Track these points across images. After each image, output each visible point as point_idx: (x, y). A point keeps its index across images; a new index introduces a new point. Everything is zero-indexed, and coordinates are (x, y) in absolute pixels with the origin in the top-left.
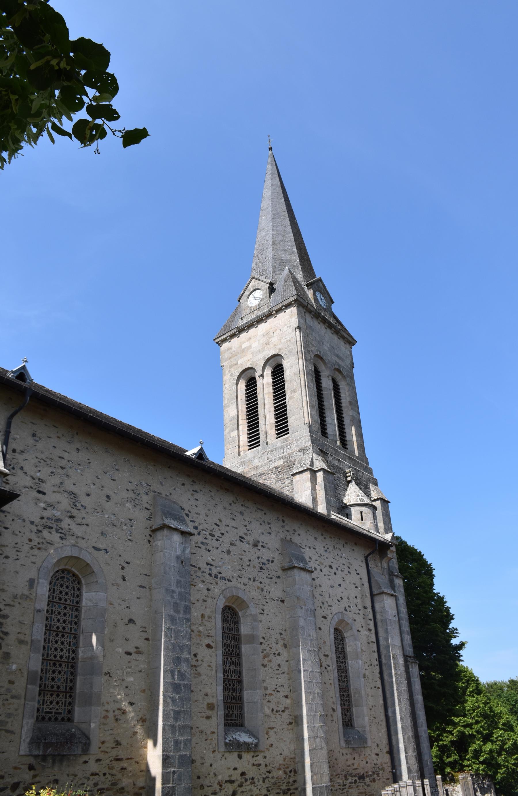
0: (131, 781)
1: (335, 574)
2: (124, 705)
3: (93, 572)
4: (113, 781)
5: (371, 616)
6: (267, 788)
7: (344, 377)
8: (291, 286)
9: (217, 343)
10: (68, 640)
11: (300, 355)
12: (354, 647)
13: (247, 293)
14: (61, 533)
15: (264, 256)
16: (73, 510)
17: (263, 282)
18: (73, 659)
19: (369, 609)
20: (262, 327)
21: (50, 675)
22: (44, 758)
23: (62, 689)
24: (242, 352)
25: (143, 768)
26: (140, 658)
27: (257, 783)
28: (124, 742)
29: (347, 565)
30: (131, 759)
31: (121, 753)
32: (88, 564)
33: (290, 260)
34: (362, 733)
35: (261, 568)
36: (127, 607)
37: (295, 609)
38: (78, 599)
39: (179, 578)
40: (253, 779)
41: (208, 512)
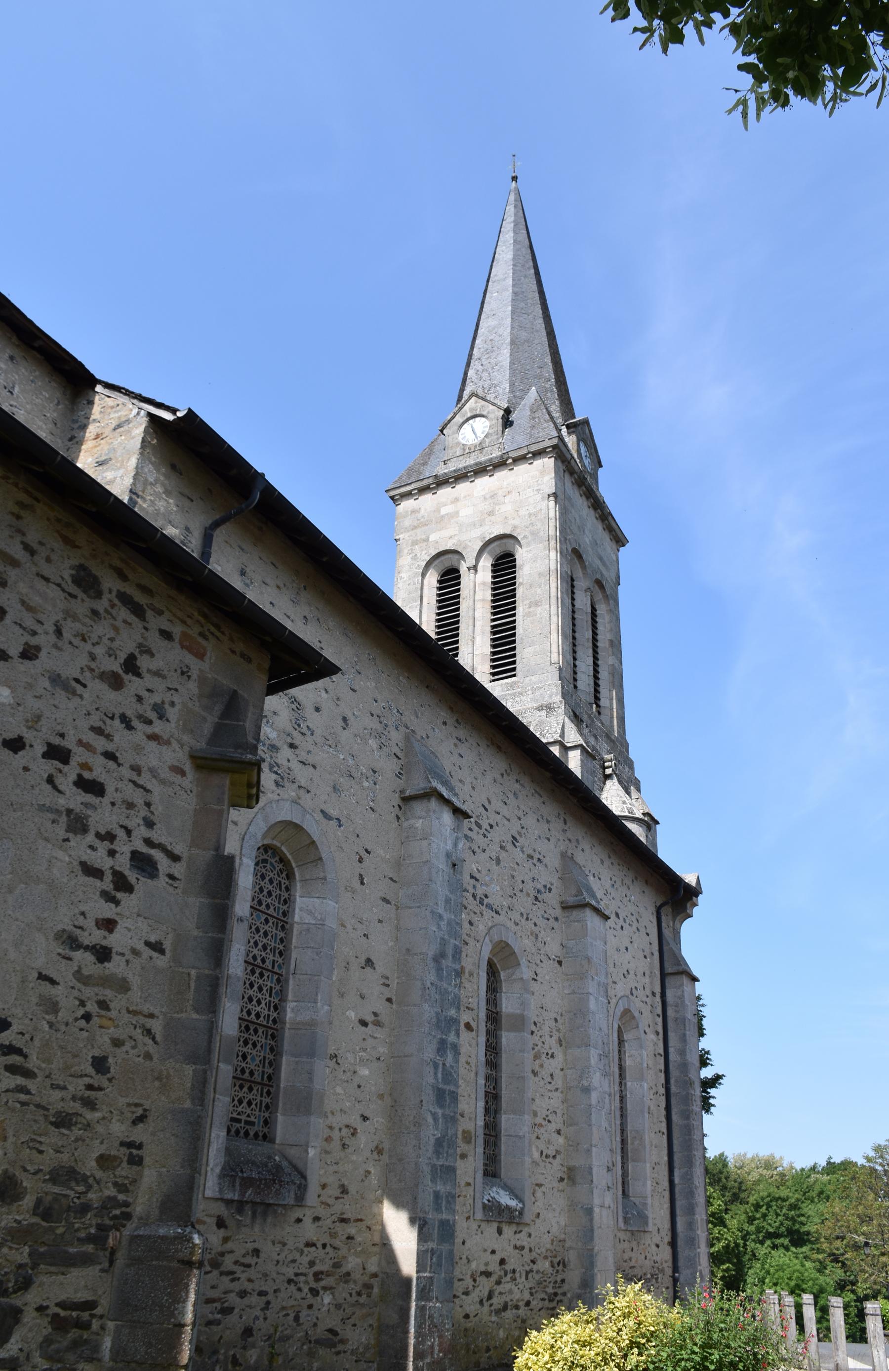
0: (359, 1260)
1: (622, 928)
2: (355, 1119)
3: (321, 859)
4: (336, 1260)
5: (659, 1010)
6: (531, 1288)
7: (606, 597)
8: (546, 421)
9: (392, 498)
10: (269, 984)
11: (553, 542)
12: (638, 1059)
13: (459, 419)
14: (276, 773)
15: (493, 361)
16: (295, 734)
17: (494, 404)
18: (275, 1021)
19: (658, 999)
20: (483, 483)
21: (241, 1049)
22: (239, 1206)
23: (257, 1077)
24: (441, 520)
25: (377, 1239)
26: (380, 1033)
27: (518, 1280)
28: (352, 1189)
29: (636, 916)
30: (361, 1220)
31: (347, 1208)
32: (313, 842)
33: (539, 377)
34: (641, 1207)
35: (536, 898)
36: (365, 935)
37: (582, 979)
38: (285, 907)
39: (448, 893)
40: (514, 1271)
41: (475, 782)
